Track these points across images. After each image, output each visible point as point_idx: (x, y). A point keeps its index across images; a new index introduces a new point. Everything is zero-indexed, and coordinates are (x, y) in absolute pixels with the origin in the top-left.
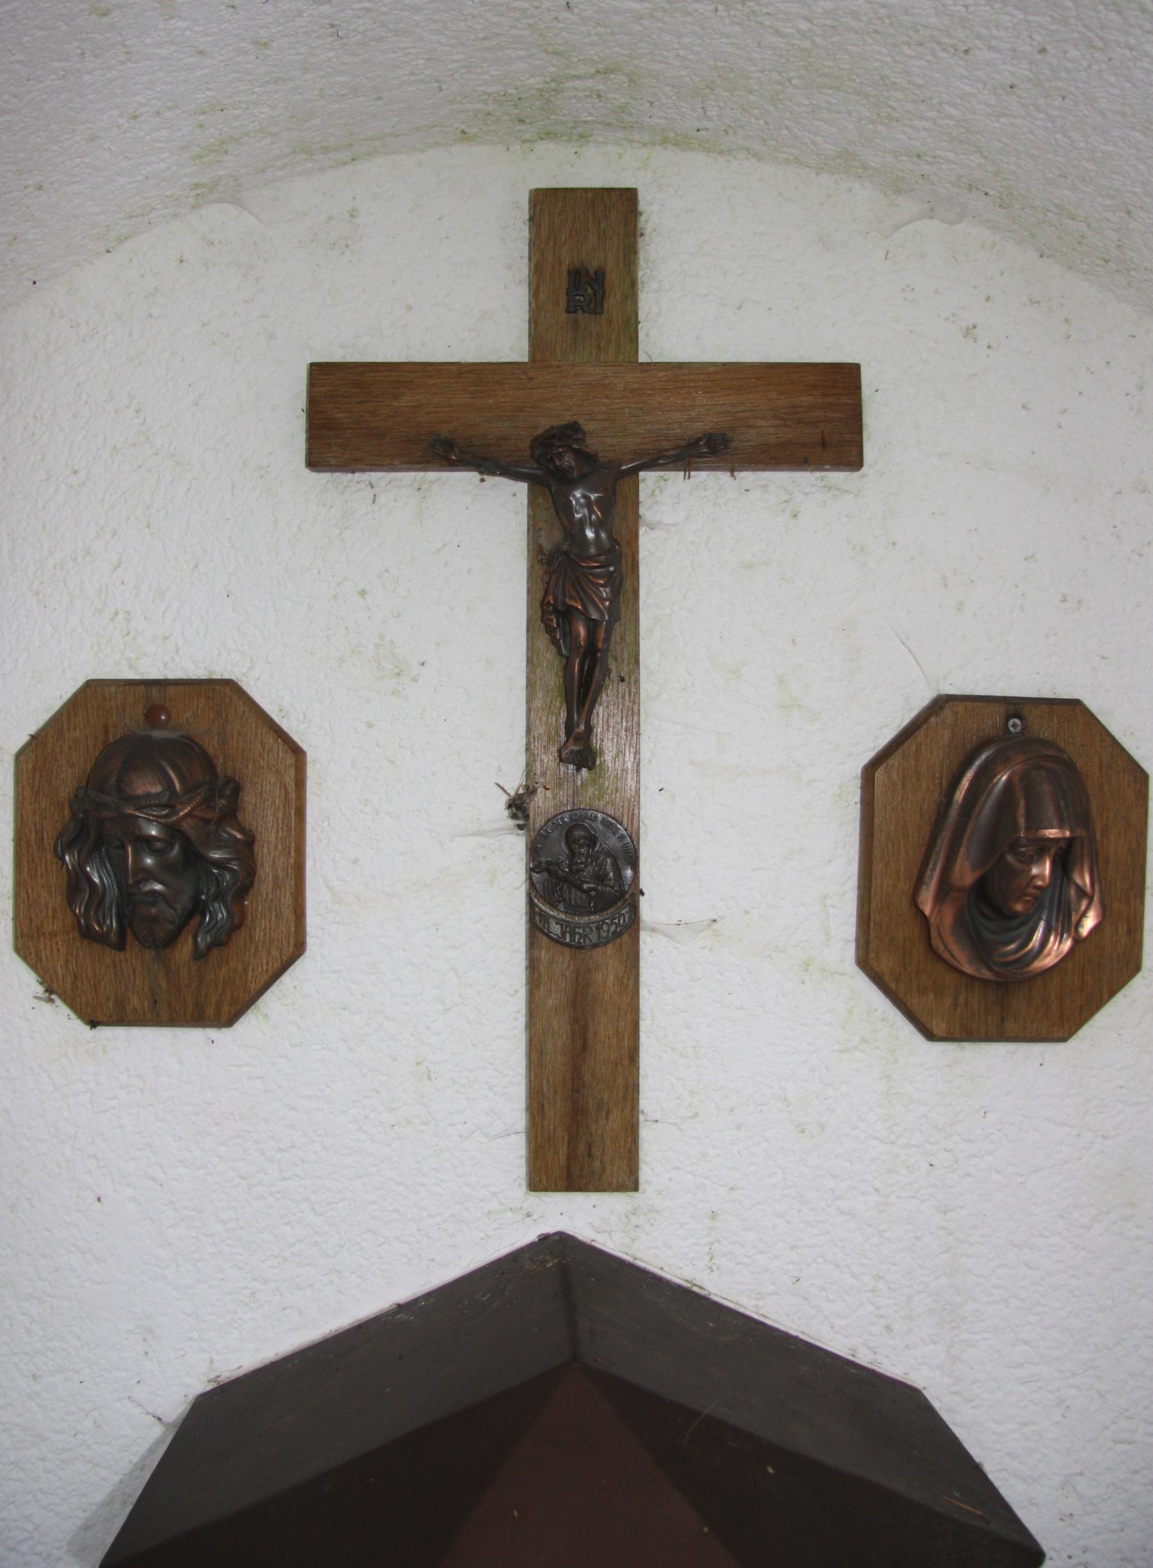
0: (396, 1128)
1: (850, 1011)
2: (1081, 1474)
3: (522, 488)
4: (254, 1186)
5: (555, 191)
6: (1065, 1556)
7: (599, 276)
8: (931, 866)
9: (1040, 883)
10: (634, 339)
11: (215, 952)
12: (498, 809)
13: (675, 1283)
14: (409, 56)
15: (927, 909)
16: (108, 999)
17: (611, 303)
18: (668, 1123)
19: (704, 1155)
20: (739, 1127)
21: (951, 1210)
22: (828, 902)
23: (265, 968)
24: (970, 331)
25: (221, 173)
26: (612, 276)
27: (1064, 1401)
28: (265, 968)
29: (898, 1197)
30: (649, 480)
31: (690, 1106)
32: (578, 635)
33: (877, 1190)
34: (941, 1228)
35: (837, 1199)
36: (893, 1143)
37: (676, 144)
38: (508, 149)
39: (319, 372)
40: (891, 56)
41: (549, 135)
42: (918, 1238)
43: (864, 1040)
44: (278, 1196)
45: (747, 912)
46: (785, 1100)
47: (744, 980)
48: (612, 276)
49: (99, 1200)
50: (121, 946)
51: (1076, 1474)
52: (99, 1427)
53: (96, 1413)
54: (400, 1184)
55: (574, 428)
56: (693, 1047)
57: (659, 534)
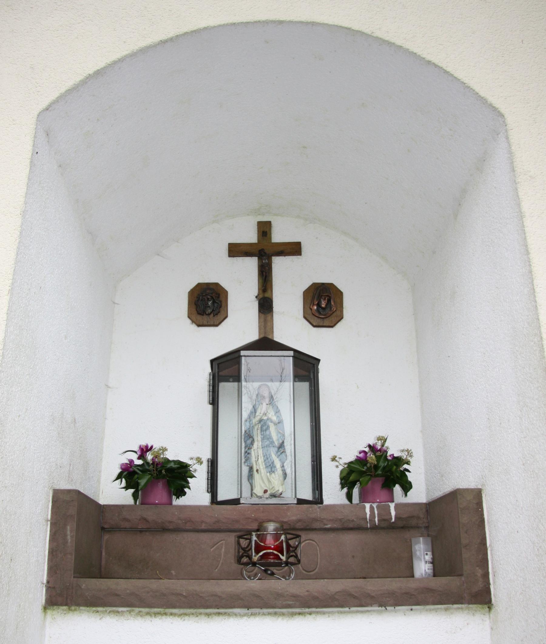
3: (256, 258)
5: (260, 222)
7: (266, 232)
10: (271, 239)
11: (216, 316)
12: (254, 297)
13: (202, 609)
15: (311, 308)
17: (268, 235)
18: (258, 444)
24: (317, 238)
25: (216, 219)
26: (268, 232)
30: (273, 258)
32: (271, 556)
37: (276, 215)
38: (268, 404)
39: (230, 244)
41: (259, 215)
48: (268, 232)
50: (203, 315)
55: (263, 249)
57: (275, 264)
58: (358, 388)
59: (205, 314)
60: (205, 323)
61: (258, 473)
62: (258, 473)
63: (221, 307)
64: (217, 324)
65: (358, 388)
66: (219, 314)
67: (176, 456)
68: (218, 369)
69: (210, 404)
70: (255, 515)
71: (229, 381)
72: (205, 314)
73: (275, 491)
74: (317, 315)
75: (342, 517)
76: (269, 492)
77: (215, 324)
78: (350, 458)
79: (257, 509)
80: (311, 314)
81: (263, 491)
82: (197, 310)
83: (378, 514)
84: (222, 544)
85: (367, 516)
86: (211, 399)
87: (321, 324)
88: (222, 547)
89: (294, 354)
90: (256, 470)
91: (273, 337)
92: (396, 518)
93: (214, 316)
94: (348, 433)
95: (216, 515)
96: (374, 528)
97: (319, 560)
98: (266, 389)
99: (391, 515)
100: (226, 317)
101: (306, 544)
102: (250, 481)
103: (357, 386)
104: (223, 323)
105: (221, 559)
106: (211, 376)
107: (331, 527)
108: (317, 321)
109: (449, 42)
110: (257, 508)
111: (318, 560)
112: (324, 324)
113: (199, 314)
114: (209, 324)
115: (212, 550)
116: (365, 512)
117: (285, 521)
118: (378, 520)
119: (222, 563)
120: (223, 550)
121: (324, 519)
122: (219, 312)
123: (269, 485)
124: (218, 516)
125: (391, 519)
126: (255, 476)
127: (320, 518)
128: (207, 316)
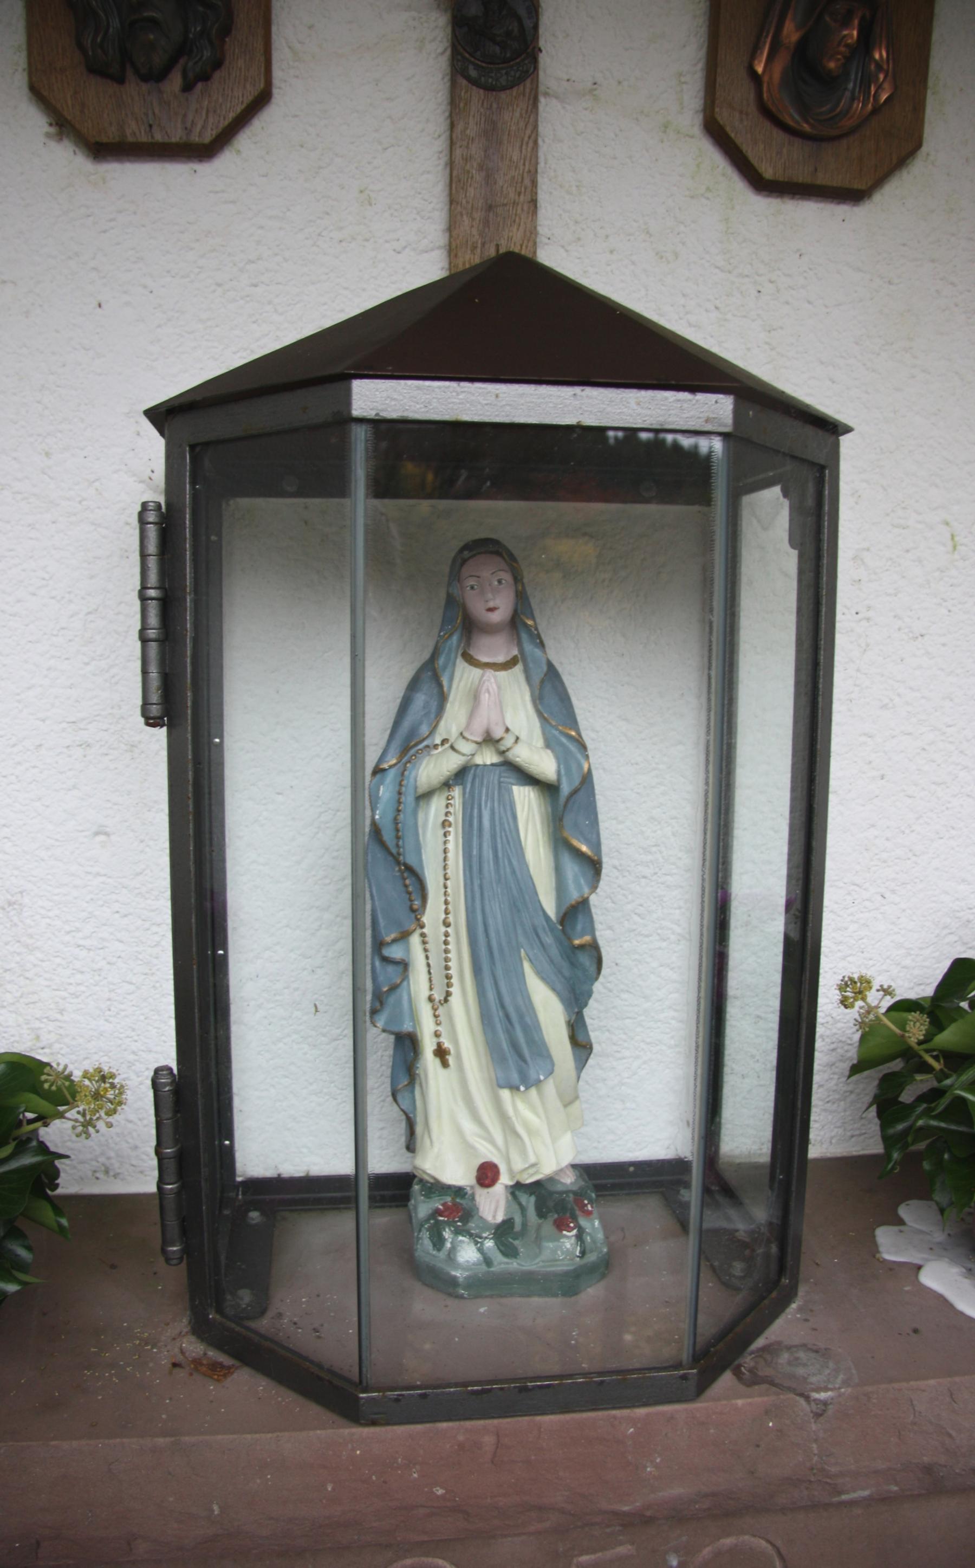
0: (344, 244)
1: (698, 166)
2: (868, 550)
4: (228, 290)
6: (854, 612)
8: (764, 34)
9: (849, 41)
14: (74, 719)
15: (760, 69)
16: (111, 124)
19: (585, 272)
20: (611, 252)
21: (774, 330)
22: (683, 79)
23: (241, 99)
27: (857, 491)
28: (241, 99)
29: (734, 315)
31: (574, 232)
33: (717, 308)
34: (767, 343)
35: (687, 313)
36: (730, 272)
40: (471, 576)
42: (749, 349)
43: (708, 189)
44: (248, 299)
45: (620, 83)
46: (648, 232)
47: (616, 135)
49: (100, 306)
50: (121, 80)
51: (864, 549)
52: (100, 494)
53: (97, 484)
54: (346, 288)
56: (577, 186)
58: (955, 547)
59: (130, 73)
60: (135, 132)
61: (445, 1064)
62: (445, 1064)
63: (226, 30)
64: (208, 138)
65: (955, 547)
66: (217, 75)
67: (10, 904)
68: (193, 483)
69: (151, 721)
71: (282, 494)
72: (130, 73)
74: (791, 116)
76: (505, 1180)
77: (195, 138)
78: (880, 898)
80: (753, 109)
82: (80, 46)
86: (155, 697)
87: (802, 175)
89: (737, 413)
90: (435, 1047)
91: (532, 235)
93: (188, 87)
94: (882, 777)
95: (216, 1508)
98: (500, 582)
100: (262, 99)
102: (405, 1104)
103: (953, 537)
104: (244, 140)
106: (152, 531)
108: (785, 151)
110: (461, 1438)
112: (822, 179)
113: (97, 69)
114: (159, 137)
122: (218, 64)
123: (506, 1142)
126: (432, 1082)
128: (145, 87)
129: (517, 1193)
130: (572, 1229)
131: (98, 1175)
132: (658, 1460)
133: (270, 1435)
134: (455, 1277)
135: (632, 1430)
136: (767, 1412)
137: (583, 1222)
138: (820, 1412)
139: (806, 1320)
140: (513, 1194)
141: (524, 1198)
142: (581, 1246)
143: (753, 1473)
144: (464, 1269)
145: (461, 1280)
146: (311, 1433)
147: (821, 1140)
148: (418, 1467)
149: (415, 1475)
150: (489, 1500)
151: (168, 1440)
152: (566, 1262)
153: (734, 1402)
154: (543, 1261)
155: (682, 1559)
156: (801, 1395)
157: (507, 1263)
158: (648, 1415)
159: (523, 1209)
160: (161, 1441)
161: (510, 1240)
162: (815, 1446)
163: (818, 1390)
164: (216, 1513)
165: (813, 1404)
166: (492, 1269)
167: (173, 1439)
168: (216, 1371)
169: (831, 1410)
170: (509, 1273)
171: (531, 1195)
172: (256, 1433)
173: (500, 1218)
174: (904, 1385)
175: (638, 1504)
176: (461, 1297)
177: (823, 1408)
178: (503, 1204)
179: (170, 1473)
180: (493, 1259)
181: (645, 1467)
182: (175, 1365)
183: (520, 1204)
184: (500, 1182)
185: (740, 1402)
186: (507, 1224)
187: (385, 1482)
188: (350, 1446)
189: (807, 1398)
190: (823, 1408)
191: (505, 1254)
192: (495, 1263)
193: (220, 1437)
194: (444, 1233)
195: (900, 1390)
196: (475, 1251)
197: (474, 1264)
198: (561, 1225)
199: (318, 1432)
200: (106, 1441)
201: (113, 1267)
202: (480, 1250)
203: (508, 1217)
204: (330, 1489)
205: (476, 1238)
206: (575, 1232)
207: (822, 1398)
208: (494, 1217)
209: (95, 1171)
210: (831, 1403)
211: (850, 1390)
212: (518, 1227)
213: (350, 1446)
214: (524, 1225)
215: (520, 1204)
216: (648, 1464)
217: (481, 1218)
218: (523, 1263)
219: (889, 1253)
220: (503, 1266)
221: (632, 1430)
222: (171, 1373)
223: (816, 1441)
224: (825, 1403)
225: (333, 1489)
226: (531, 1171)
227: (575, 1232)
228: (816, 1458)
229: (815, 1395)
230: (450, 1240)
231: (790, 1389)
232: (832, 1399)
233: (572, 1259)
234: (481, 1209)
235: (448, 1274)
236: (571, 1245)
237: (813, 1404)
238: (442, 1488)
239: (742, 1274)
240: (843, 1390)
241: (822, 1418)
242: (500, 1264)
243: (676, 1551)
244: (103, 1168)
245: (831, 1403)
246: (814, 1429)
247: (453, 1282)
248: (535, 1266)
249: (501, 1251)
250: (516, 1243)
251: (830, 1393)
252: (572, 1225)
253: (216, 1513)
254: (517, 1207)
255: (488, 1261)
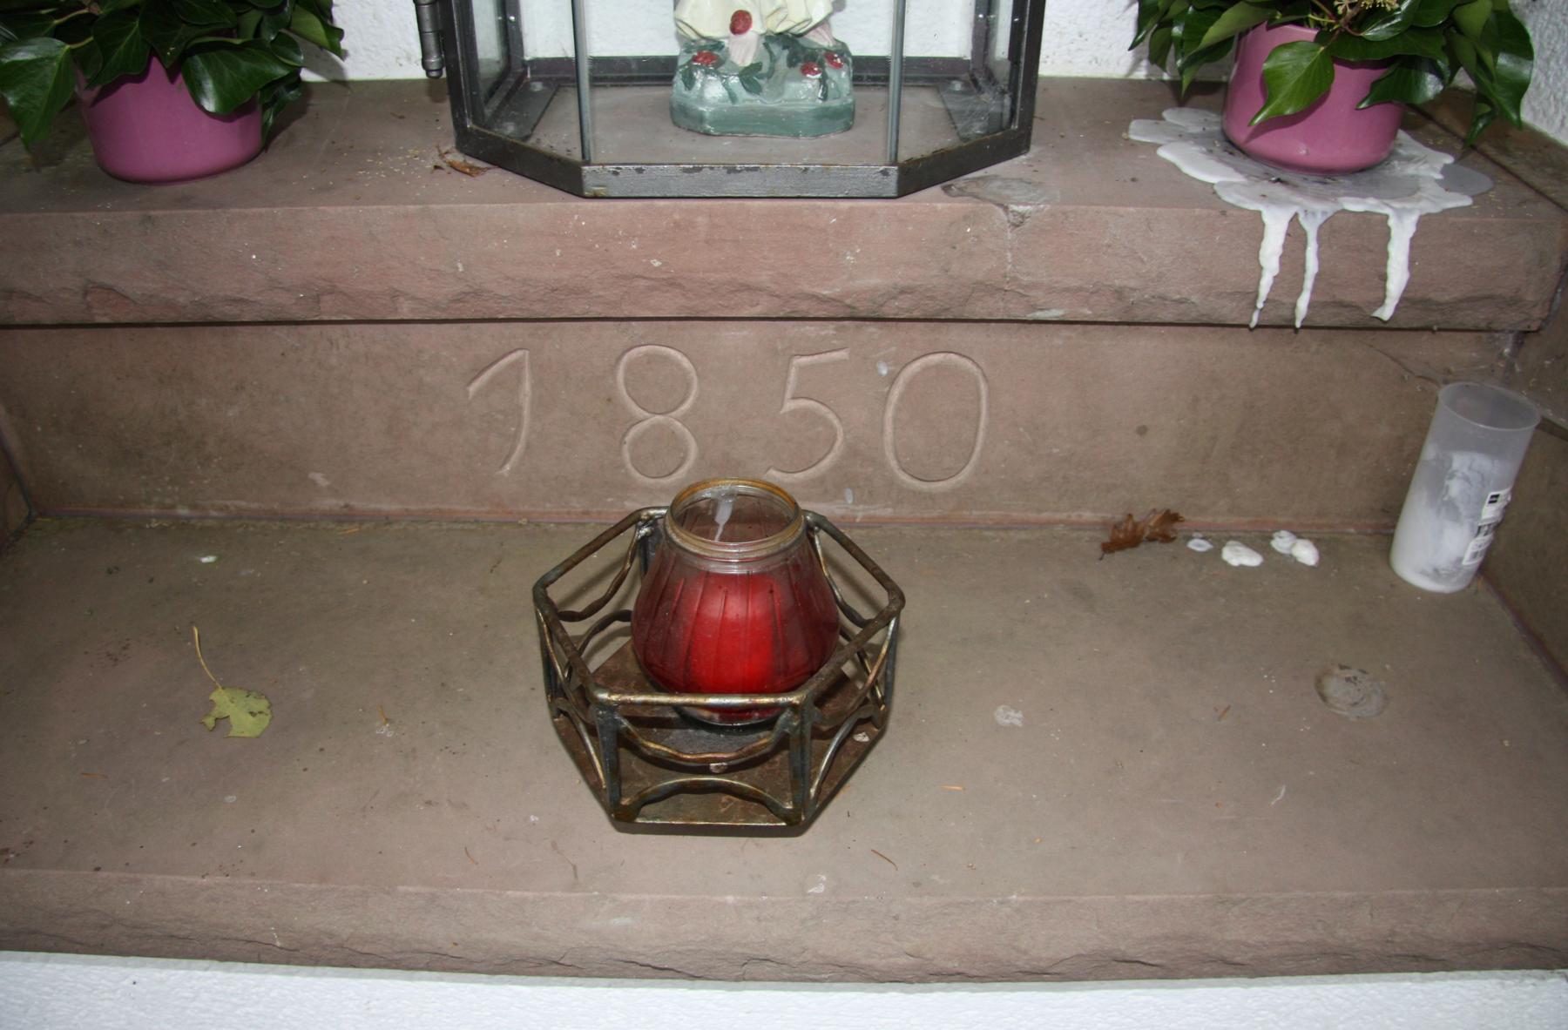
70: (665, 264)
73: (791, 24)
75: (1132, 284)
76: (757, 28)
79: (677, 224)
81: (729, 22)
83: (1318, 277)
84: (517, 365)
85: (1258, 284)
88: (519, 380)
92: (1405, 301)
95: (461, 267)
96: (1280, 326)
97: (981, 434)
99: (1384, 289)
101: (926, 369)
105: (519, 426)
107: (1063, 316)
109: (18, 855)
110: (677, 217)
111: (976, 434)
115: (473, 389)
116: (1258, 261)
117: (824, 296)
118: (1311, 306)
119: (528, 446)
120: (527, 386)
121: (1034, 286)
124: (467, 266)
125: (1381, 302)
127: (1015, 279)
129: (770, 45)
130: (817, 73)
131: (402, 61)
132: (858, 251)
133: (505, 205)
134: (702, 112)
135: (834, 220)
136: (965, 218)
137: (830, 71)
138: (1019, 222)
139: (1031, 166)
140: (766, 45)
141: (776, 49)
142: (823, 89)
143: (947, 271)
144: (713, 105)
145: (707, 115)
146: (542, 204)
147: (1107, 60)
148: (636, 239)
149: (634, 247)
150: (701, 275)
151: (418, 207)
152: (808, 102)
153: (934, 204)
154: (786, 101)
155: (891, 368)
156: (1000, 205)
157: (752, 101)
158: (851, 208)
159: (773, 59)
160: (411, 208)
161: (755, 78)
162: (1009, 255)
163: (1018, 204)
164: (460, 270)
165: (1011, 215)
166: (736, 105)
167: (421, 207)
168: (472, 172)
169: (1028, 223)
170: (753, 110)
171: (784, 48)
172: (493, 203)
173: (748, 63)
174: (1103, 208)
175: (838, 290)
176: (707, 134)
177: (1020, 219)
178: (753, 50)
179: (421, 236)
180: (738, 96)
181: (845, 255)
182: (436, 167)
183: (771, 53)
184: (751, 29)
185: (940, 206)
186: (756, 67)
187: (606, 250)
188: (576, 217)
189: (1006, 209)
190: (1020, 219)
191: (748, 90)
192: (740, 100)
193: (462, 206)
194: (695, 74)
195: (1098, 212)
196: (721, 87)
197: (719, 100)
198: (806, 70)
199: (549, 204)
200: (366, 207)
201: (401, 117)
202: (725, 86)
203: (758, 61)
204: (558, 254)
205: (723, 78)
206: (819, 76)
207: (1020, 211)
208: (743, 61)
209: (398, 58)
210: (1029, 217)
211: (1048, 207)
212: (765, 70)
213: (576, 217)
214: (772, 70)
215: (771, 53)
216: (849, 253)
217: (732, 62)
218: (766, 101)
219: (1136, 134)
220: (747, 103)
221: (834, 220)
222: (432, 172)
223: (1011, 249)
224: (1023, 216)
225: (561, 255)
226: (781, 15)
227: (819, 76)
228: (1010, 266)
229: (1014, 207)
230: (701, 81)
231: (990, 201)
232: (1030, 213)
233: (814, 100)
234: (733, 55)
235: (696, 110)
236: (813, 86)
237: (1011, 215)
238: (659, 260)
239: (954, 82)
240: (1042, 206)
241: (1018, 229)
242: (744, 101)
243: (886, 360)
244: (404, 54)
245: (1029, 217)
246: (1009, 238)
247: (701, 118)
248: (777, 105)
249: (745, 88)
250: (761, 82)
251: (1029, 207)
252: (816, 69)
253: (460, 270)
254: (767, 54)
255: (732, 97)
